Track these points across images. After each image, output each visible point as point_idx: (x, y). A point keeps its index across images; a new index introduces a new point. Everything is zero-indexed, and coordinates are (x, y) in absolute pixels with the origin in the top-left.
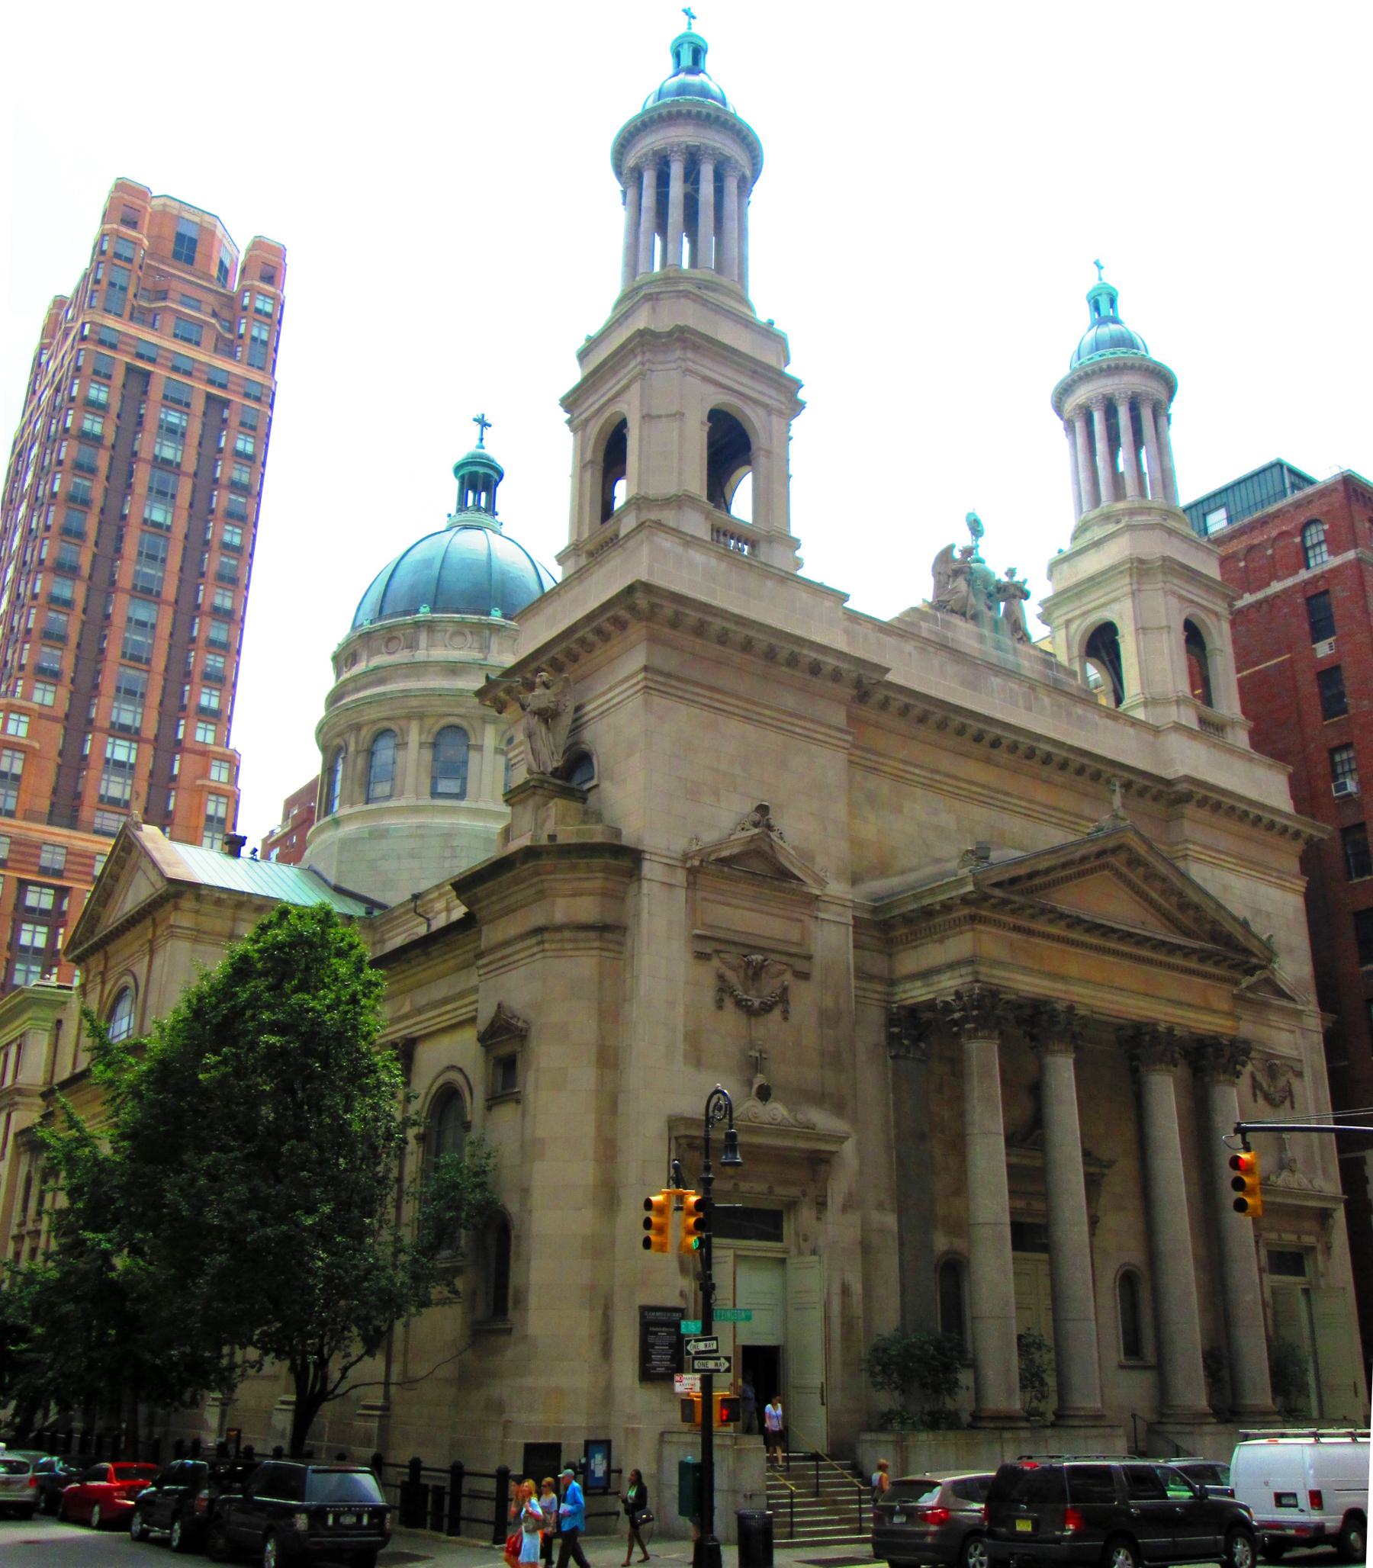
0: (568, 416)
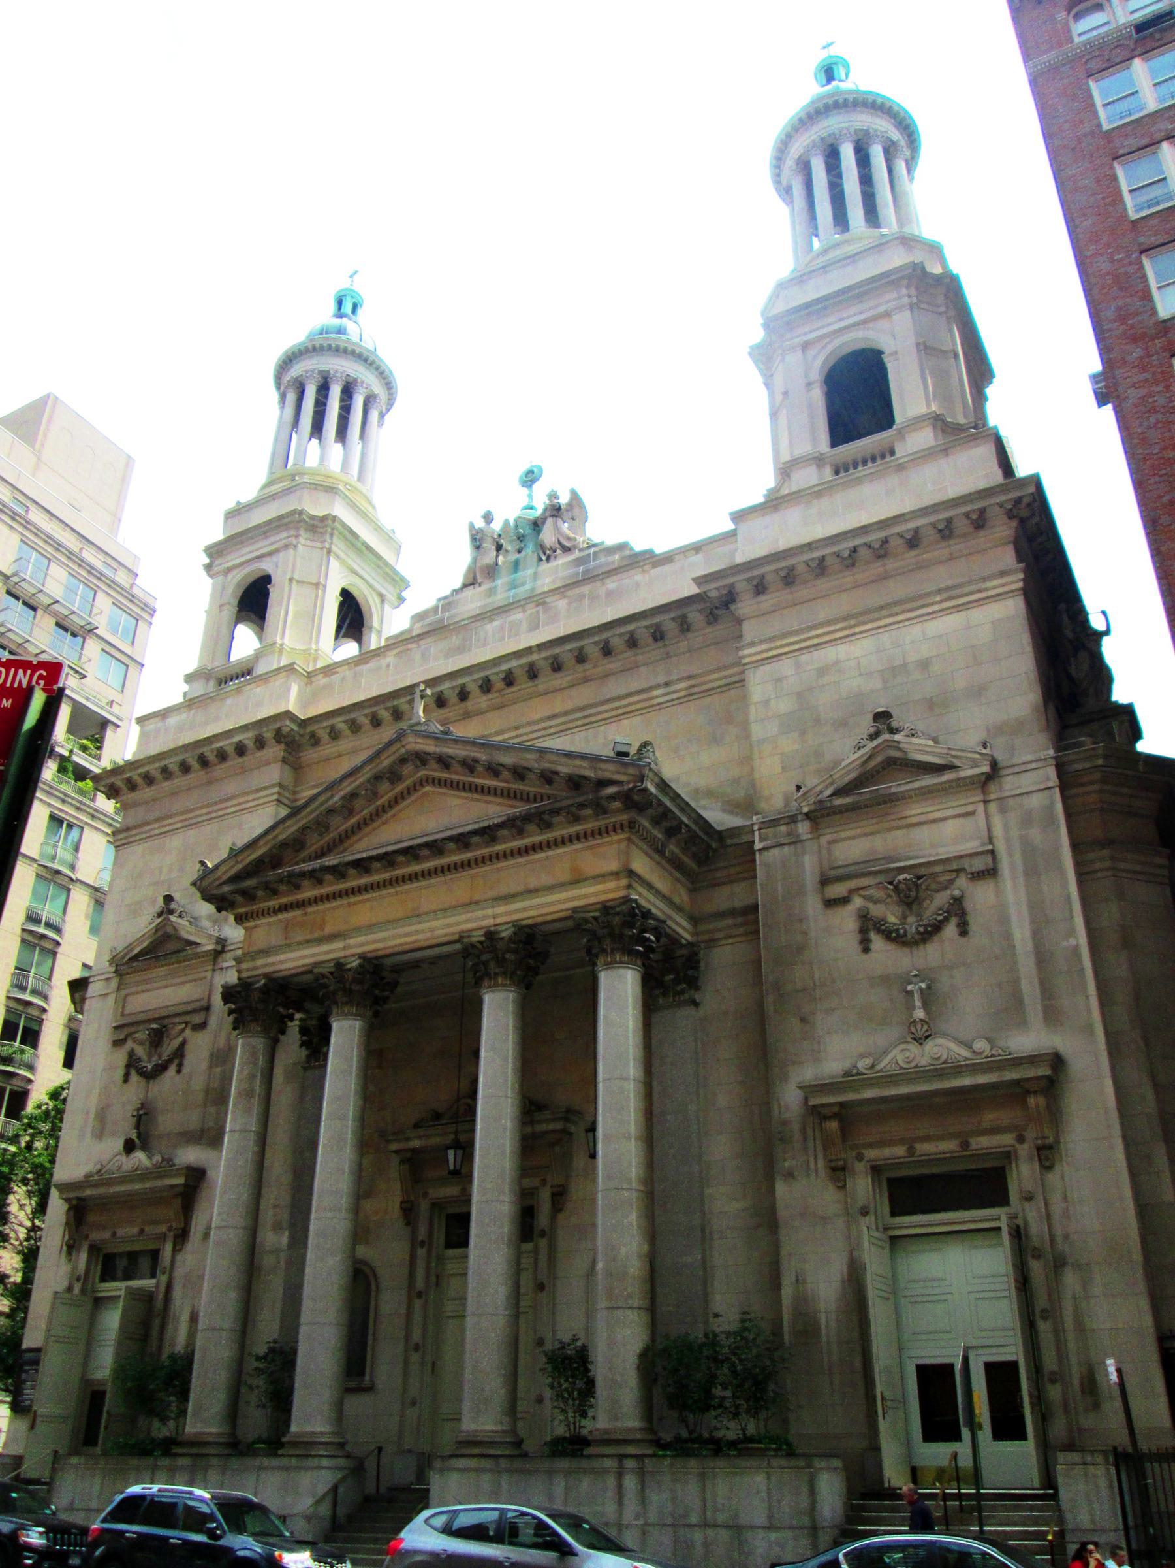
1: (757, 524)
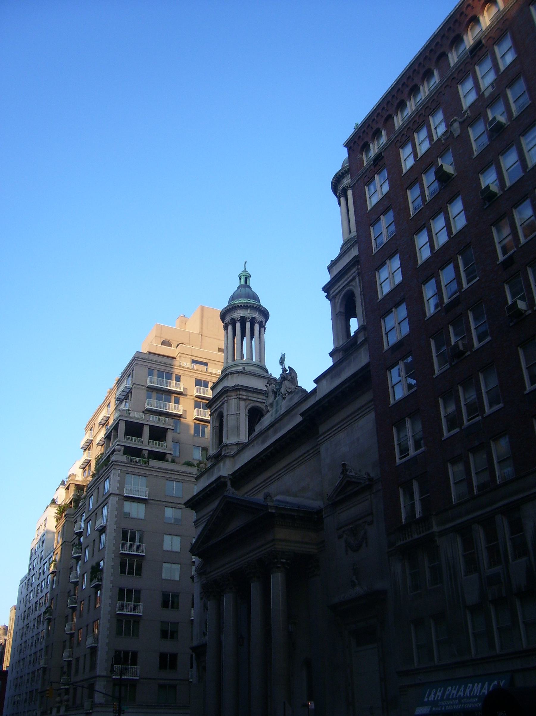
0: (326, 294)
1: (324, 382)
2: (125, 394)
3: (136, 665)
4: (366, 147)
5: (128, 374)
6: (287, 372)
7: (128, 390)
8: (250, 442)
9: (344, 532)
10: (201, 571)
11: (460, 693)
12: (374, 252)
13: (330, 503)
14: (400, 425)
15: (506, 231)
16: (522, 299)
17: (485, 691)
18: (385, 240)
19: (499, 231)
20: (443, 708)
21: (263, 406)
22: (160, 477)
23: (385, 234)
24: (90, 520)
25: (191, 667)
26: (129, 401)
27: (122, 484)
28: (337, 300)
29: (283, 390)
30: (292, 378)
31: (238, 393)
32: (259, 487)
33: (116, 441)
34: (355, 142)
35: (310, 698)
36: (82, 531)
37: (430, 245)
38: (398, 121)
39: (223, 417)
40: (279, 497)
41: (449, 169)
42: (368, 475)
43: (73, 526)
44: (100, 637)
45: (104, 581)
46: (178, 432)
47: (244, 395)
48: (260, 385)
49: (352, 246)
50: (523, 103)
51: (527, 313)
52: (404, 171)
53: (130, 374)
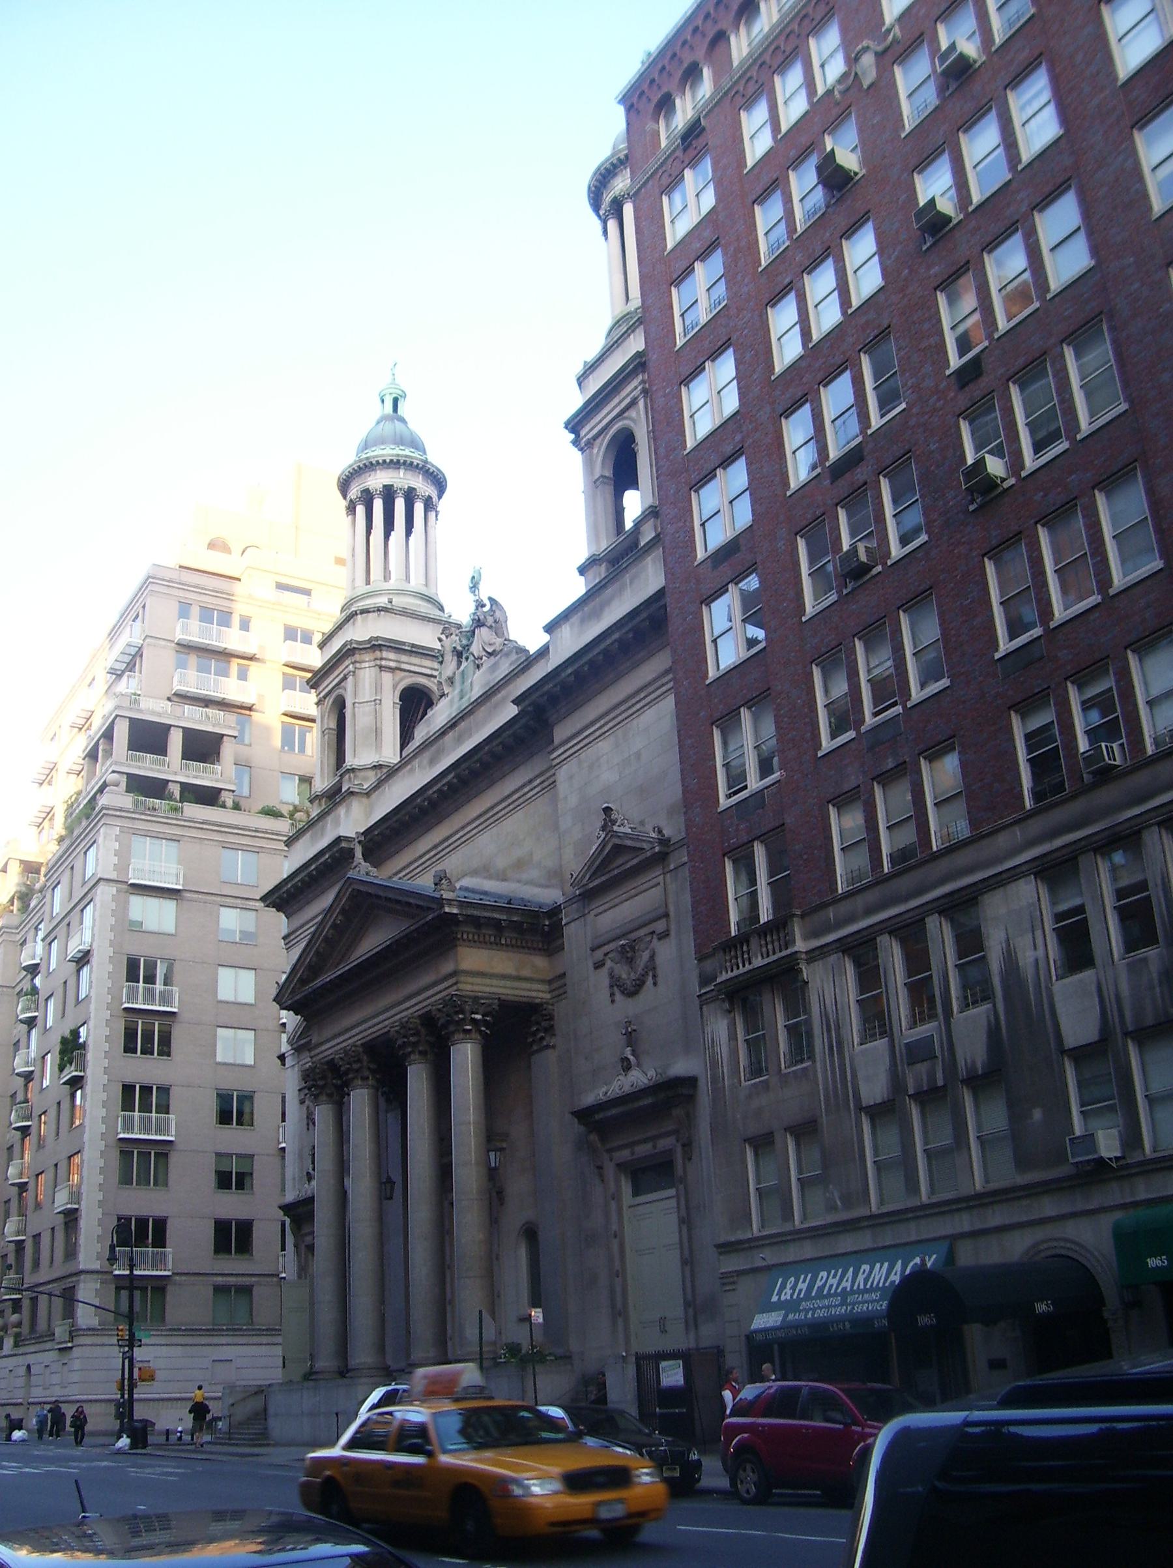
0: (573, 436)
1: (565, 630)
2: (127, 659)
3: (164, 1247)
4: (665, 105)
5: (133, 614)
6: (486, 609)
7: (133, 651)
8: (404, 763)
9: (606, 955)
10: (301, 1045)
11: (844, 1284)
12: (679, 344)
13: (577, 892)
14: (728, 721)
15: (969, 301)
16: (998, 452)
17: (896, 1278)
18: (704, 319)
19: (952, 301)
20: (810, 1315)
21: (431, 684)
22: (206, 842)
23: (703, 303)
24: (55, 938)
25: (283, 1249)
26: (137, 674)
27: (124, 856)
28: (595, 451)
29: (475, 649)
30: (495, 621)
31: (378, 654)
32: (424, 859)
33: (108, 763)
34: (643, 93)
35: (535, 1304)
36: (39, 961)
37: (801, 330)
38: (741, 46)
39: (344, 707)
40: (467, 882)
41: (849, 160)
42: (660, 832)
43: (15, 1002)
44: (84, 1189)
45: (89, 1071)
46: (247, 742)
47: (390, 660)
48: (427, 637)
49: (631, 330)
50: (1017, 12)
51: (1006, 485)
52: (750, 163)
53: (137, 616)
